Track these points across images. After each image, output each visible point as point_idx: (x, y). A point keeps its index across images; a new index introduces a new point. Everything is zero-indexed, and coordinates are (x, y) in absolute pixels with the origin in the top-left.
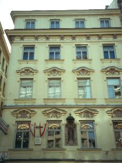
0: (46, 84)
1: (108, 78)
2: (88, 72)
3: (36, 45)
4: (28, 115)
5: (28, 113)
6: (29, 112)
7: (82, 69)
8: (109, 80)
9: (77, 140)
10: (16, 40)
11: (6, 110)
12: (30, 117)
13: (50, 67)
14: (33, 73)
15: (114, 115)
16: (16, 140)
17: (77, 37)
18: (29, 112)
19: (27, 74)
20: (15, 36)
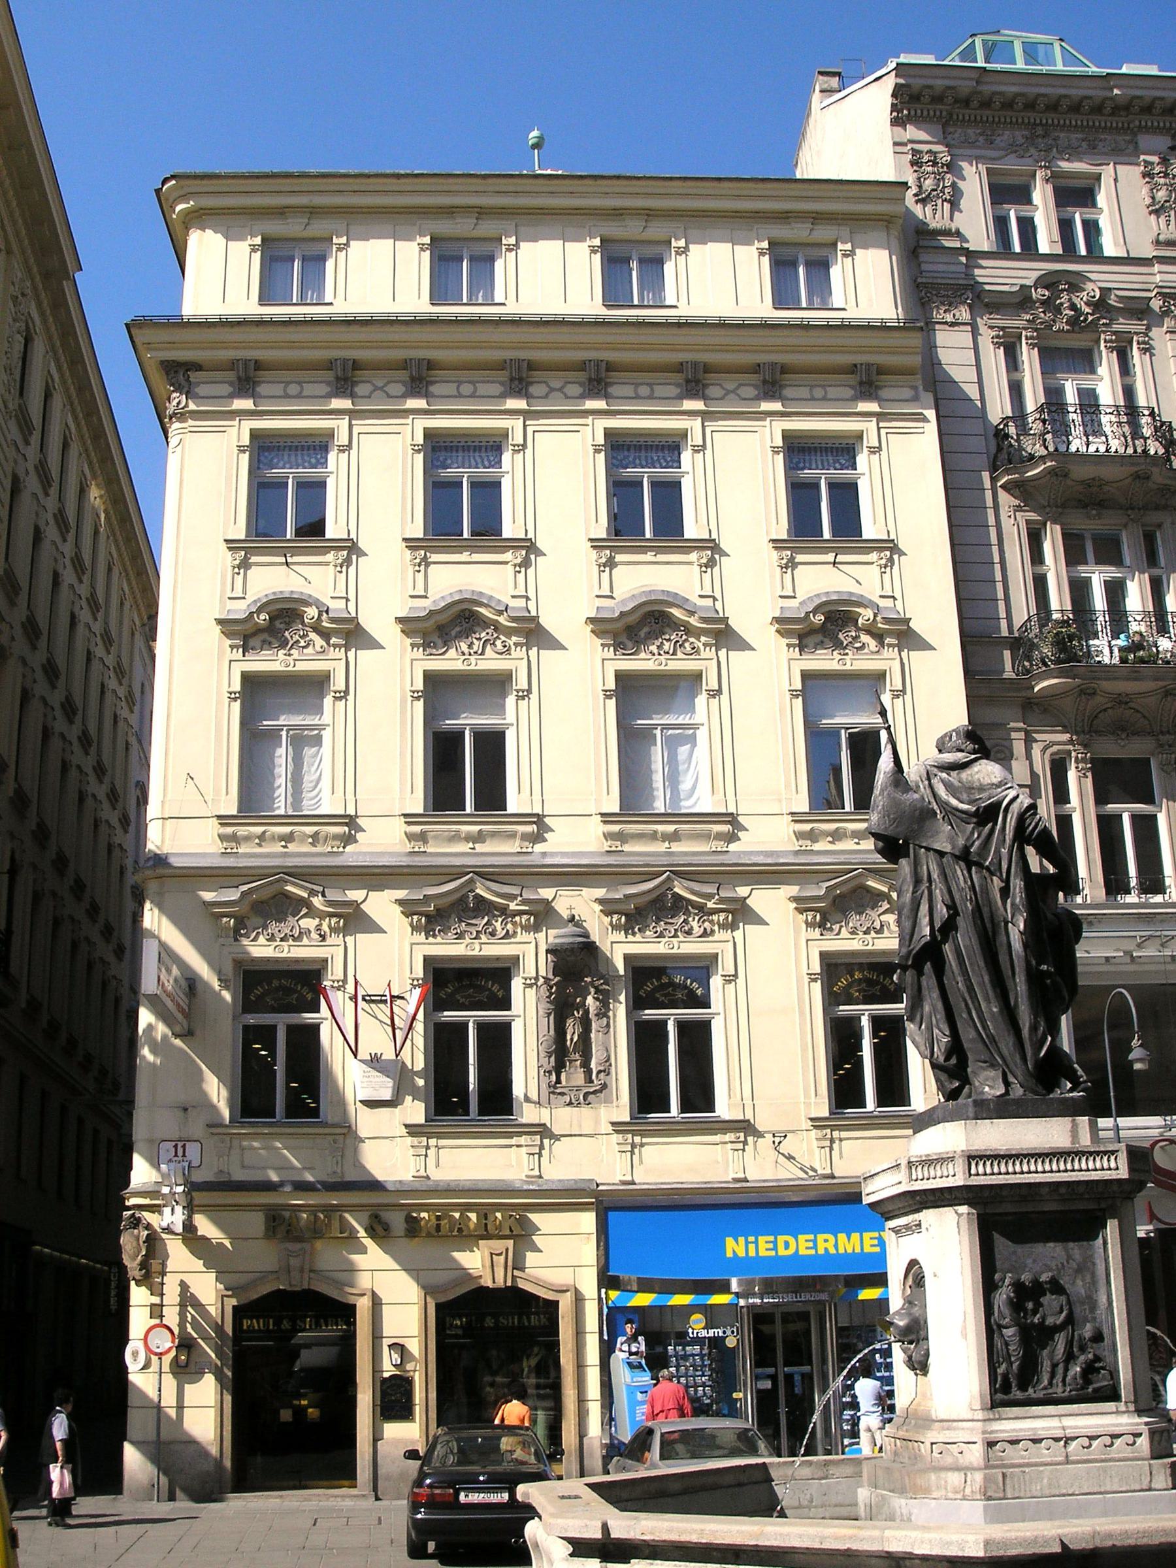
7: (651, 614)
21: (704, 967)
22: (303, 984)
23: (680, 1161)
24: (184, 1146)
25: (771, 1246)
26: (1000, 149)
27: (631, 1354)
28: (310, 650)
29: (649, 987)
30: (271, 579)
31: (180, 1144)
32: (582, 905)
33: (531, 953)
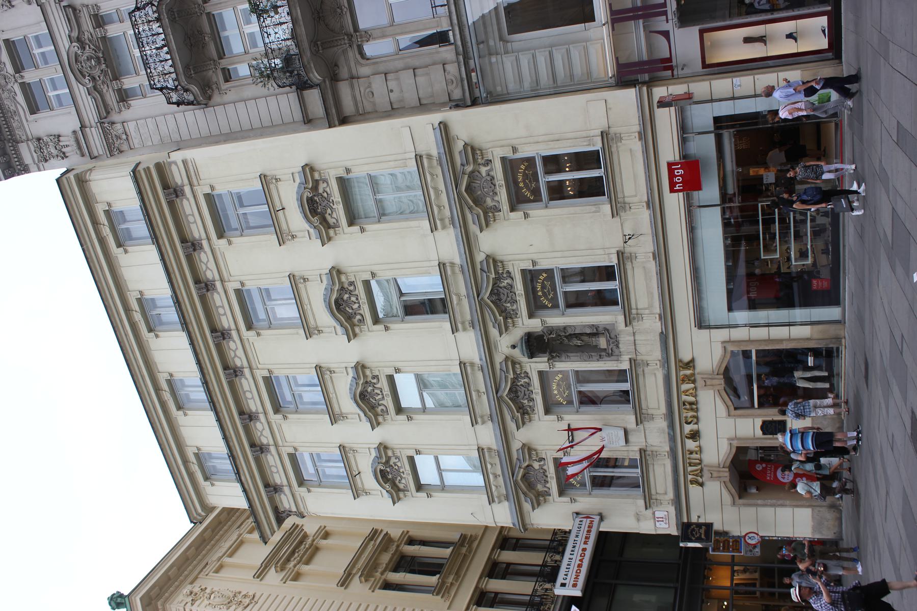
4: (536, 465)
6: (469, 168)
7: (338, 309)
12: (542, 459)
13: (306, 226)
16: (596, 305)
19: (328, 199)
21: (510, 165)
28: (399, 464)
29: (528, 194)
30: (295, 219)
32: (506, 344)
33: (536, 366)
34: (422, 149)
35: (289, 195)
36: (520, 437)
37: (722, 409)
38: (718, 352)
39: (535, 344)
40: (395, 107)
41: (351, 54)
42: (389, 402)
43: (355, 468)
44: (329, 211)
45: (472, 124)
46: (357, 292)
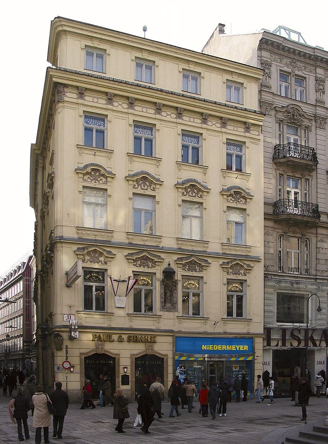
0: (180, 212)
1: (229, 208)
2: (199, 190)
3: (158, 125)
4: (102, 259)
5: (101, 254)
8: (137, 199)
9: (176, 303)
10: (68, 94)
11: (64, 245)
12: (106, 263)
14: (106, 178)
15: (230, 271)
17: (229, 123)
18: (105, 253)
20: (66, 86)
22: (101, 275)
23: (192, 326)
24: (70, 316)
25: (243, 348)
26: (283, 64)
27: (180, 371)
28: (101, 182)
31: (69, 315)
34: (210, 244)
35: (100, 160)
36: (120, 255)
37: (135, 352)
38: (164, 353)
39: (169, 274)
40: (317, 248)
41: (281, 231)
42: (139, 191)
43: (100, 154)
44: (233, 199)
45: (258, 271)
46: (188, 196)
